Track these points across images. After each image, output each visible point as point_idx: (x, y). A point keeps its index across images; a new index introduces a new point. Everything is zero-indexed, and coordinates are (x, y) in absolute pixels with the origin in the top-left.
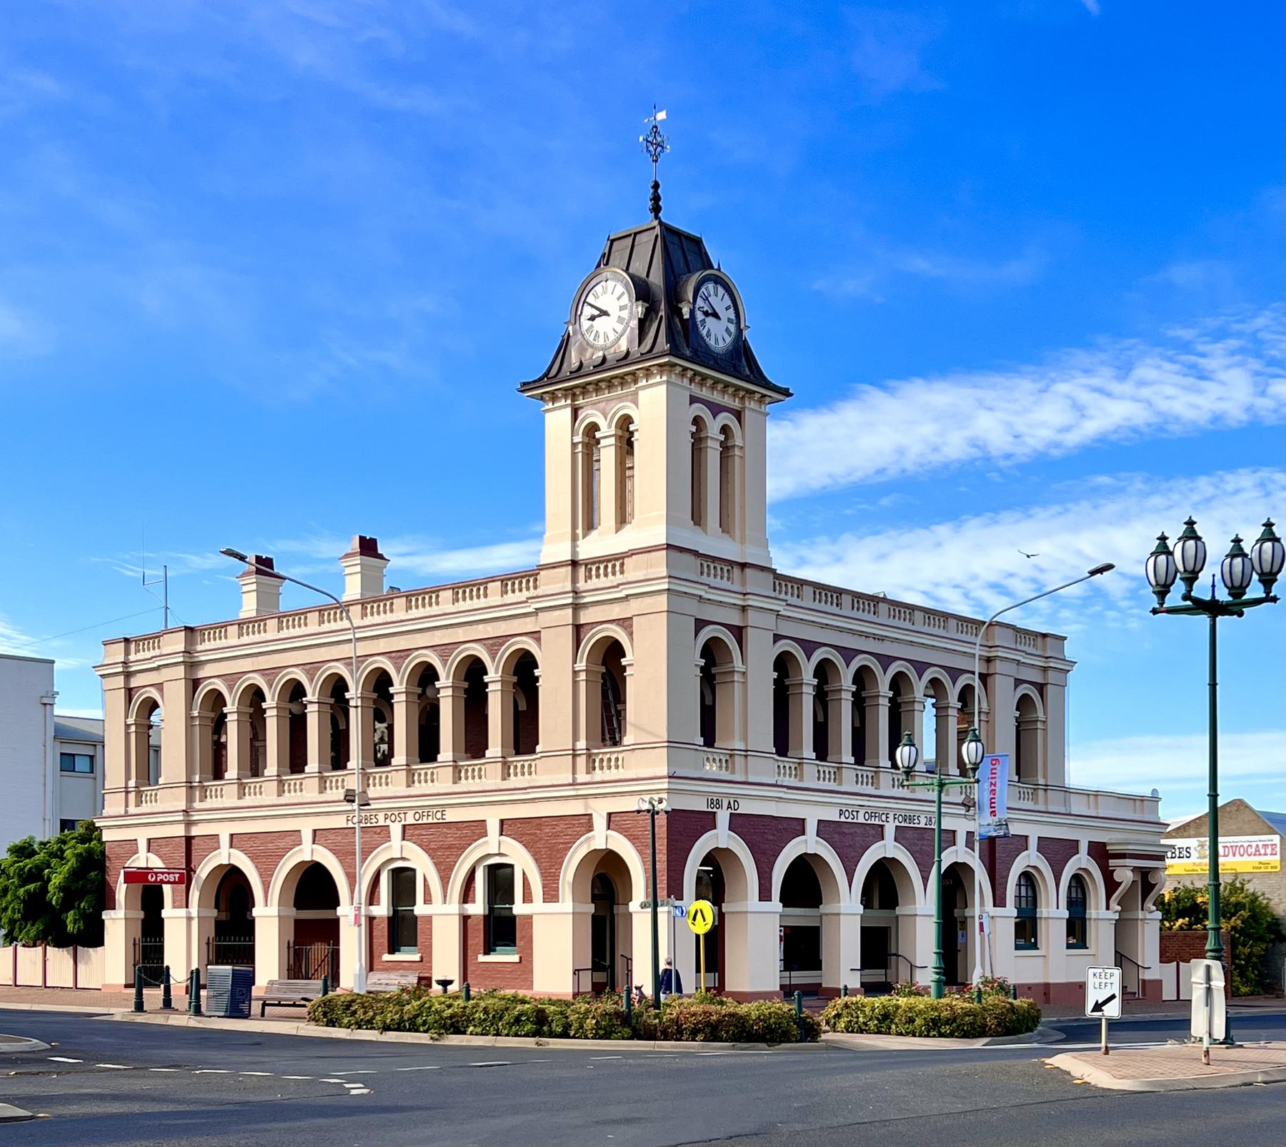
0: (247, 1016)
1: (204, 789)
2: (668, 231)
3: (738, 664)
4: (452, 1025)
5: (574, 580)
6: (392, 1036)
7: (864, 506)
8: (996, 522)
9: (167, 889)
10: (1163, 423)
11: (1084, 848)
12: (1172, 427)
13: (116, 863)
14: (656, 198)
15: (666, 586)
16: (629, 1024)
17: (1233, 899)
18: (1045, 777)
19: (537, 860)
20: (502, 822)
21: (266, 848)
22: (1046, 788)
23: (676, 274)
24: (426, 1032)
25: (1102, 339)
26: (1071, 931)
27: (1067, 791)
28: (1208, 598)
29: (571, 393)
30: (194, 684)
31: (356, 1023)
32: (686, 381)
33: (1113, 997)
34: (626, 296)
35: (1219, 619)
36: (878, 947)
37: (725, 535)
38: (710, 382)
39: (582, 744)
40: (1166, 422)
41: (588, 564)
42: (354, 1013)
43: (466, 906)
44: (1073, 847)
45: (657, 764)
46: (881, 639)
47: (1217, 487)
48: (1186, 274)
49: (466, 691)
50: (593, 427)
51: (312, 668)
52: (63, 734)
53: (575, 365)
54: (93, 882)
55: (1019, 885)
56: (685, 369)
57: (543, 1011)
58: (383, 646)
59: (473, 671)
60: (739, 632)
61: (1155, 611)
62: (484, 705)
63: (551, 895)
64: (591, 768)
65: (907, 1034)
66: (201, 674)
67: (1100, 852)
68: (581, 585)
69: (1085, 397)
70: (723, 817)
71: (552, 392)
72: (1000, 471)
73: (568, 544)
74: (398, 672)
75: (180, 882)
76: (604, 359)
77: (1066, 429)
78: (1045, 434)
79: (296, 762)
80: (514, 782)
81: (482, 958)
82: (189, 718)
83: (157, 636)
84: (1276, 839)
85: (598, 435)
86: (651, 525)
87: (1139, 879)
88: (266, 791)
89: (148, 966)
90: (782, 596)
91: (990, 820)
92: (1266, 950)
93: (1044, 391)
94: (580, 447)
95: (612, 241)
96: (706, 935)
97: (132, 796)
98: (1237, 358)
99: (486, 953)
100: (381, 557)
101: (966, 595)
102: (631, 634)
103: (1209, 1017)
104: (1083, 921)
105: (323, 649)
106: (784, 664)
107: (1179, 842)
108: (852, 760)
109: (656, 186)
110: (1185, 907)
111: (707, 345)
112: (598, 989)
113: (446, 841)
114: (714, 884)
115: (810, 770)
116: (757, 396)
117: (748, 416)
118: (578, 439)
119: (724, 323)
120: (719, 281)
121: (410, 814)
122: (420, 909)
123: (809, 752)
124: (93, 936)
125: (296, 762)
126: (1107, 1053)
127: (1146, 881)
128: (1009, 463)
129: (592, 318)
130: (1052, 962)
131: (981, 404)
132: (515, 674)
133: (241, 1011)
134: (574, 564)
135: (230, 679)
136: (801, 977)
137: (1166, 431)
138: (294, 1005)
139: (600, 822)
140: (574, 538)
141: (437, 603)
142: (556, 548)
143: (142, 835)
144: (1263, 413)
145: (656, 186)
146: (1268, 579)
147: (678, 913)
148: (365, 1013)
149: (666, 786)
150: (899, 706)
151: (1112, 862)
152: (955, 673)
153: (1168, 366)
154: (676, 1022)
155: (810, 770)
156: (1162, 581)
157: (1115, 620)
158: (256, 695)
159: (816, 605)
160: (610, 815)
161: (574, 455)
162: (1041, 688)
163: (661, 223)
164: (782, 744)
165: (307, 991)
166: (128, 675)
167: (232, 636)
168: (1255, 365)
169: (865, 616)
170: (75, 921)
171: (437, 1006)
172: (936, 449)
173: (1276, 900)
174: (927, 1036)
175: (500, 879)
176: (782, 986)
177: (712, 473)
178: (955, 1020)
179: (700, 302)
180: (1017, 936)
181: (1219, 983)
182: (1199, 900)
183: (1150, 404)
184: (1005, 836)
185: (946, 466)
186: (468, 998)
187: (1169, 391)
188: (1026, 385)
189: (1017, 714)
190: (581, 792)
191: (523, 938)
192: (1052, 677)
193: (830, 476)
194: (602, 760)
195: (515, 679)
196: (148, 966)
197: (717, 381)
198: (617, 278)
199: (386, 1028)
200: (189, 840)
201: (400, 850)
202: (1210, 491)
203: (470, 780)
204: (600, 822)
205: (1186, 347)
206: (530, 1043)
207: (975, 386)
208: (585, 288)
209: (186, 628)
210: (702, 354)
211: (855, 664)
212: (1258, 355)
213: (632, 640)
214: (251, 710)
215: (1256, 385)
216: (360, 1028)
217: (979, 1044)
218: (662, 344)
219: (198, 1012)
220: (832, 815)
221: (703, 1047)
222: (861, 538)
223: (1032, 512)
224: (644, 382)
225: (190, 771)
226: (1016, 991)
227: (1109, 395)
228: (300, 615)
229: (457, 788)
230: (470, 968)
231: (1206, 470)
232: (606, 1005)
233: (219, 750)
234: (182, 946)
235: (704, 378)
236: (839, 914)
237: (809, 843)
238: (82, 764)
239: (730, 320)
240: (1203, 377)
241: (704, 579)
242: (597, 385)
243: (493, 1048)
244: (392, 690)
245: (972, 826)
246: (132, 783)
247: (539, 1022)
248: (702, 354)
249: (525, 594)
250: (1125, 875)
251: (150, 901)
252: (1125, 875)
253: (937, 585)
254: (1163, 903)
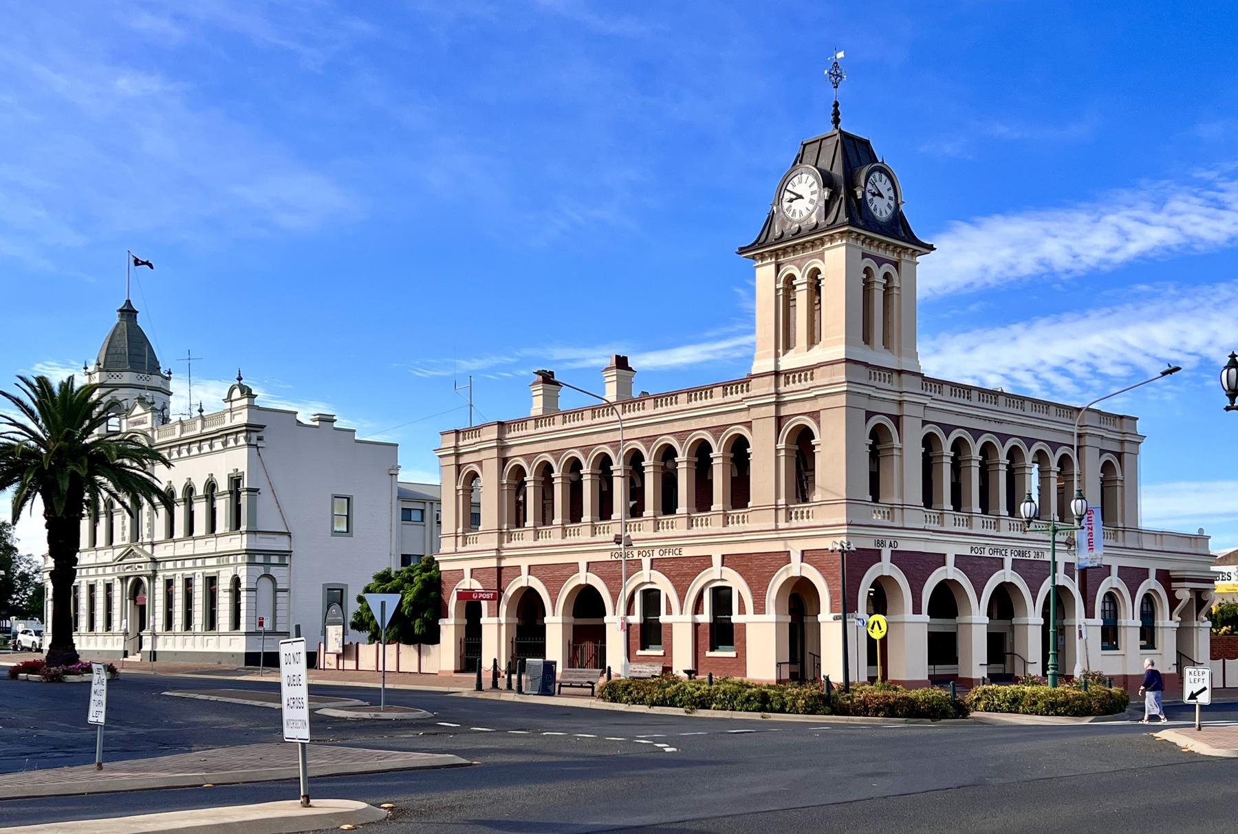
0: (552, 695)
1: (510, 534)
2: (845, 137)
5: (777, 385)
6: (657, 710)
8: (1059, 321)
9: (484, 604)
11: (1152, 574)
12: (1197, 247)
14: (836, 114)
18: (1123, 521)
19: (749, 584)
20: (723, 556)
21: (554, 575)
22: (1124, 530)
23: (852, 169)
27: (1140, 532)
29: (775, 254)
30: (504, 461)
32: (859, 243)
33: (1205, 689)
36: (999, 648)
38: (876, 243)
39: (782, 501)
41: (787, 373)
42: (630, 693)
44: (1144, 573)
45: (839, 515)
46: (1000, 422)
48: (1210, 131)
49: (696, 464)
51: (586, 449)
52: (405, 495)
53: (778, 234)
55: (1104, 602)
56: (859, 234)
57: (766, 693)
58: (637, 433)
60: (897, 420)
61: (1227, 409)
62: (709, 474)
63: (760, 609)
64: (789, 518)
65: (1031, 713)
66: (509, 454)
67: (1165, 577)
68: (782, 389)
69: (1129, 225)
70: (886, 554)
72: (1062, 283)
73: (773, 360)
76: (800, 228)
77: (1114, 250)
78: (1097, 254)
79: (575, 514)
80: (732, 528)
81: (708, 654)
82: (501, 485)
85: (794, 283)
86: (833, 346)
88: (553, 536)
89: (470, 656)
90: (928, 393)
93: (1097, 221)
94: (781, 292)
97: (460, 539)
99: (643, 649)
100: (630, 369)
101: (1036, 377)
102: (818, 423)
106: (929, 442)
108: (980, 511)
109: (836, 105)
113: (682, 570)
115: (949, 519)
117: (903, 265)
118: (780, 286)
119: (886, 200)
120: (883, 170)
121: (657, 551)
123: (948, 506)
126: (1199, 729)
127: (1200, 599)
128: (1069, 276)
129: (791, 201)
131: (1047, 233)
134: (777, 373)
135: (529, 457)
136: (942, 670)
137: (1192, 249)
139: (796, 557)
140: (777, 356)
142: (763, 363)
143: (467, 567)
145: (836, 105)
147: (860, 623)
150: (1013, 470)
151: (1174, 585)
152: (1055, 446)
153: (1194, 200)
154: (863, 702)
155: (949, 519)
157: (1153, 394)
158: (546, 469)
159: (953, 399)
160: (803, 552)
162: (1119, 456)
163: (841, 131)
166: (458, 455)
169: (988, 406)
170: (420, 627)
172: (1012, 267)
175: (722, 598)
176: (930, 676)
177: (879, 309)
178: (1067, 703)
179: (869, 186)
180: (1103, 640)
183: (1180, 229)
185: (1020, 280)
186: (711, 683)
188: (1082, 218)
193: (930, 289)
195: (732, 455)
196: (470, 656)
197: (881, 242)
198: (810, 172)
199: (653, 704)
201: (648, 576)
202: (1229, 294)
204: (796, 557)
205: (1208, 185)
206: (757, 716)
207: (1043, 220)
208: (786, 180)
216: (634, 703)
217: (1086, 721)
218: (843, 217)
219: (520, 691)
220: (966, 551)
222: (954, 335)
224: (829, 245)
225: (500, 522)
226: (1111, 680)
227: (1147, 223)
228: (578, 412)
230: (700, 661)
233: (520, 508)
234: (495, 642)
237: (949, 572)
238: (416, 516)
239: (890, 198)
241: (872, 382)
242: (794, 249)
244: (643, 464)
246: (460, 530)
247: (763, 700)
249: (740, 396)
250: (1184, 595)
252: (1184, 595)
253: (1013, 369)
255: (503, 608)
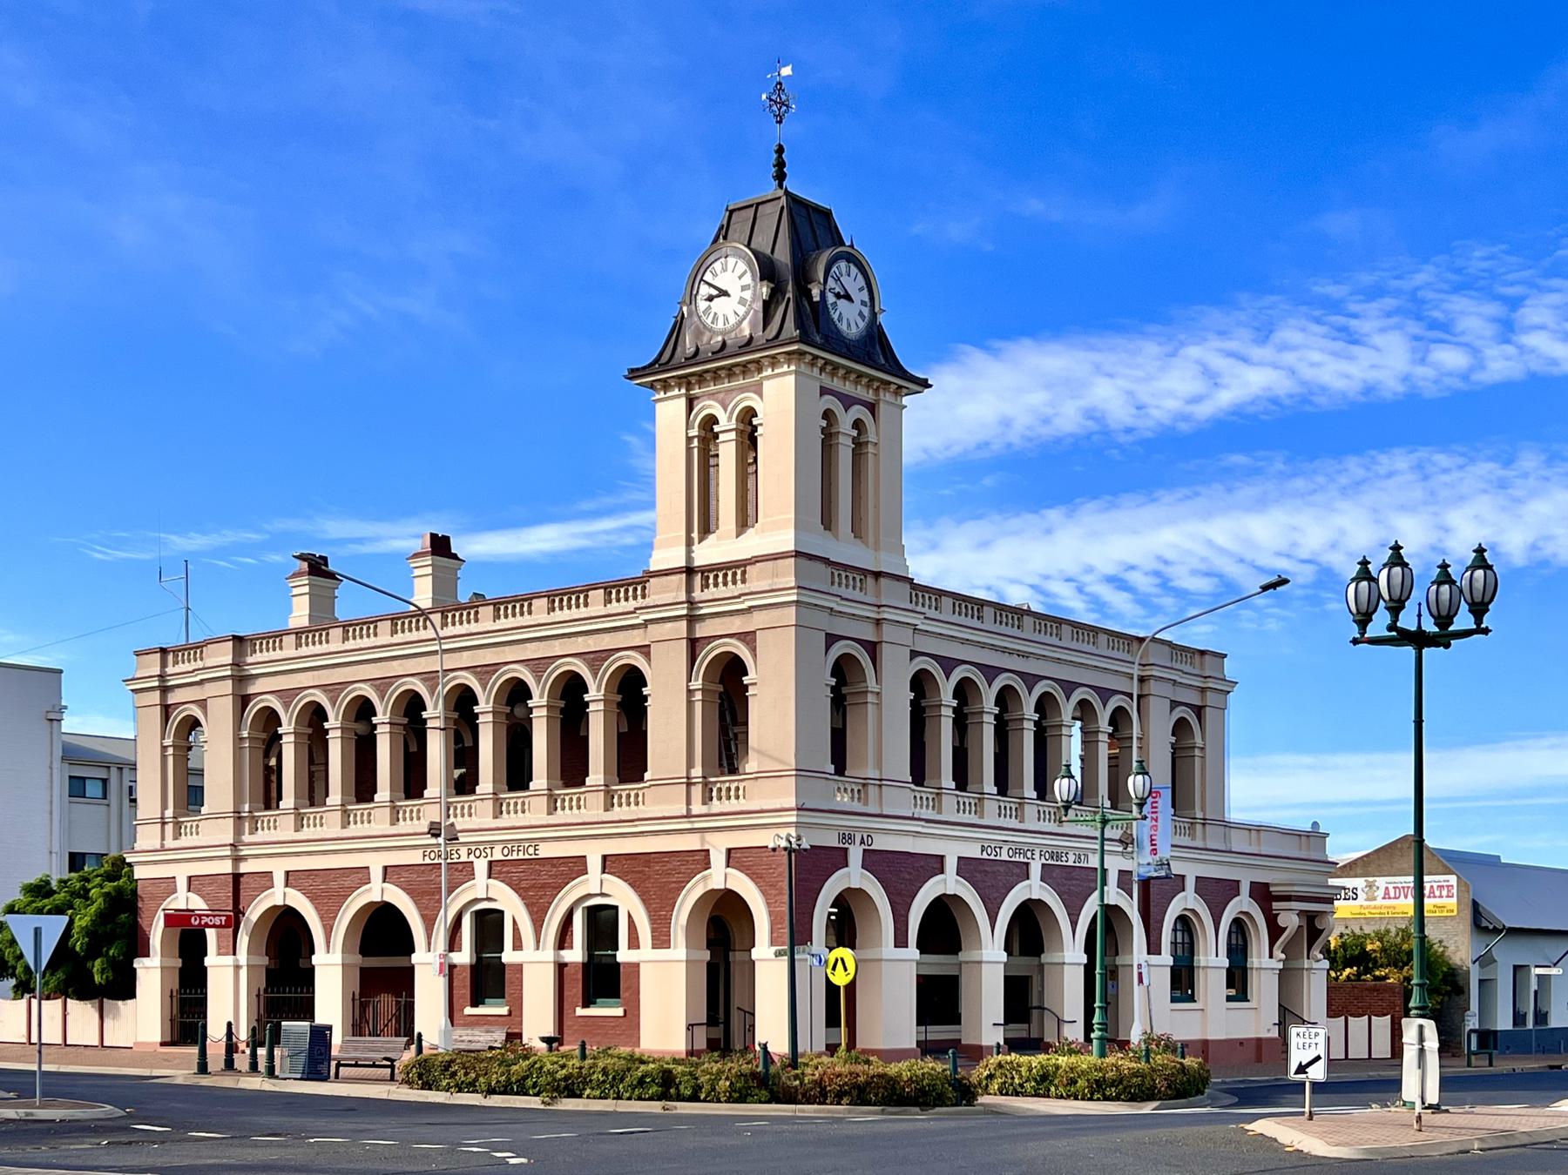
0: (325, 1079)
1: (254, 820)
2: (795, 203)
3: (871, 684)
4: (566, 1087)
6: (497, 1101)
7: (963, 486)
9: (211, 934)
10: (1308, 394)
11: (1245, 889)
12: (1320, 400)
13: (152, 904)
14: (780, 164)
15: (794, 598)
16: (766, 1083)
17: (1405, 947)
18: (1203, 809)
21: (329, 887)
24: (537, 1095)
25: (1243, 297)
26: (1230, 984)
27: (1227, 825)
28: (1413, 628)
29: (685, 381)
30: (243, 701)
31: (456, 1085)
32: (816, 370)
33: (1318, 1058)
34: (749, 275)
35: (1425, 651)
36: (1021, 998)
37: (858, 541)
38: (841, 372)
39: (697, 771)
40: (1312, 394)
41: (706, 570)
42: (454, 1074)
43: (563, 953)
45: (784, 795)
47: (1368, 469)
48: (1340, 223)
49: (562, 711)
50: (711, 420)
51: (382, 684)
52: (73, 754)
53: (690, 350)
54: (123, 925)
55: (1175, 930)
56: (816, 357)
57: (670, 1071)
58: (467, 659)
59: (571, 690)
60: (872, 648)
61: (1355, 642)
62: (583, 727)
63: (661, 939)
65: (1068, 1097)
66: (251, 690)
67: (1262, 894)
68: (697, 595)
69: (1218, 362)
70: (855, 854)
71: (665, 380)
72: (1119, 447)
73: (682, 549)
74: (484, 689)
75: (227, 926)
77: (1196, 400)
78: (1172, 404)
79: (363, 788)
81: (580, 1011)
82: (238, 740)
83: (200, 646)
84: (1453, 879)
85: (716, 429)
86: (777, 530)
87: (1304, 924)
89: (186, 1019)
90: (919, 608)
91: (1150, 859)
92: (1441, 1003)
93: (1173, 354)
95: (731, 212)
96: (846, 987)
98: (1394, 320)
99: (586, 1005)
100: (455, 557)
101: (1080, 590)
102: (753, 651)
103: (1420, 1077)
104: (1244, 970)
105: (395, 663)
106: (921, 683)
107: (1348, 882)
109: (780, 150)
110: (1353, 955)
111: (838, 331)
112: (712, 1045)
113: (539, 879)
114: (844, 930)
116: (893, 387)
117: (882, 407)
118: (694, 432)
120: (851, 258)
121: (498, 848)
122: (508, 956)
124: (124, 988)
125: (363, 788)
126: (1311, 1118)
127: (1313, 929)
128: (1129, 438)
129: (710, 298)
130: (1214, 1018)
131: (1098, 369)
132: (619, 692)
133: (319, 1073)
134: (690, 571)
135: (287, 695)
136: (938, 1033)
137: (1310, 403)
138: (374, 1066)
139: (718, 859)
140: (689, 543)
141: (530, 613)
142: (668, 555)
143: (181, 873)
144: (1421, 383)
145: (780, 150)
146: (1479, 610)
147: (816, 962)
148: (466, 1074)
149: (794, 819)
151: (1275, 905)
152: (1105, 694)
153: (1315, 328)
154: (819, 1083)
156: (1364, 608)
158: (316, 715)
161: (689, 450)
162: (1199, 711)
163: (787, 193)
164: (919, 772)
165: (388, 1050)
166: (165, 690)
167: (289, 648)
168: (1414, 328)
170: (102, 972)
171: (549, 1066)
172: (1046, 421)
173: (1452, 948)
174: (1091, 1099)
175: (602, 923)
176: (919, 1043)
177: (845, 469)
181: (1432, 1043)
182: (1369, 947)
183: (1292, 372)
184: (1167, 877)
185: (1058, 440)
186: (584, 1057)
187: (1316, 356)
188: (1152, 348)
189: (1173, 739)
190: (697, 825)
191: (628, 989)
192: (1211, 698)
193: (925, 451)
194: (720, 790)
195: (619, 698)
196: (186, 1019)
197: (849, 371)
199: (491, 1091)
200: (237, 877)
201: (483, 889)
202: (1361, 473)
203: (575, 810)
204: (718, 859)
205: (1335, 306)
206: (655, 1107)
207: (1092, 348)
209: (235, 638)
210: (832, 340)
211: (999, 683)
212: (1419, 318)
213: (755, 656)
214: (310, 731)
215: (1414, 351)
217: (1148, 1108)
218: (791, 330)
219: (271, 1072)
220: (973, 851)
221: (849, 1112)
223: (1156, 495)
226: (1185, 1048)
227: (1245, 360)
229: (553, 820)
230: (567, 1023)
231: (1357, 451)
232: (737, 1065)
235: (836, 367)
236: (980, 962)
237: (948, 883)
238: (93, 789)
239: (863, 303)
240: (1355, 342)
241: (835, 589)
242: (716, 375)
243: (615, 1113)
244: (476, 709)
245: (1127, 865)
246: (169, 813)
248: (832, 340)
249: (632, 604)
250: (1290, 920)
251: (190, 943)
252: (1290, 920)
253: (1047, 577)
254: (1328, 951)
255: (243, 940)
